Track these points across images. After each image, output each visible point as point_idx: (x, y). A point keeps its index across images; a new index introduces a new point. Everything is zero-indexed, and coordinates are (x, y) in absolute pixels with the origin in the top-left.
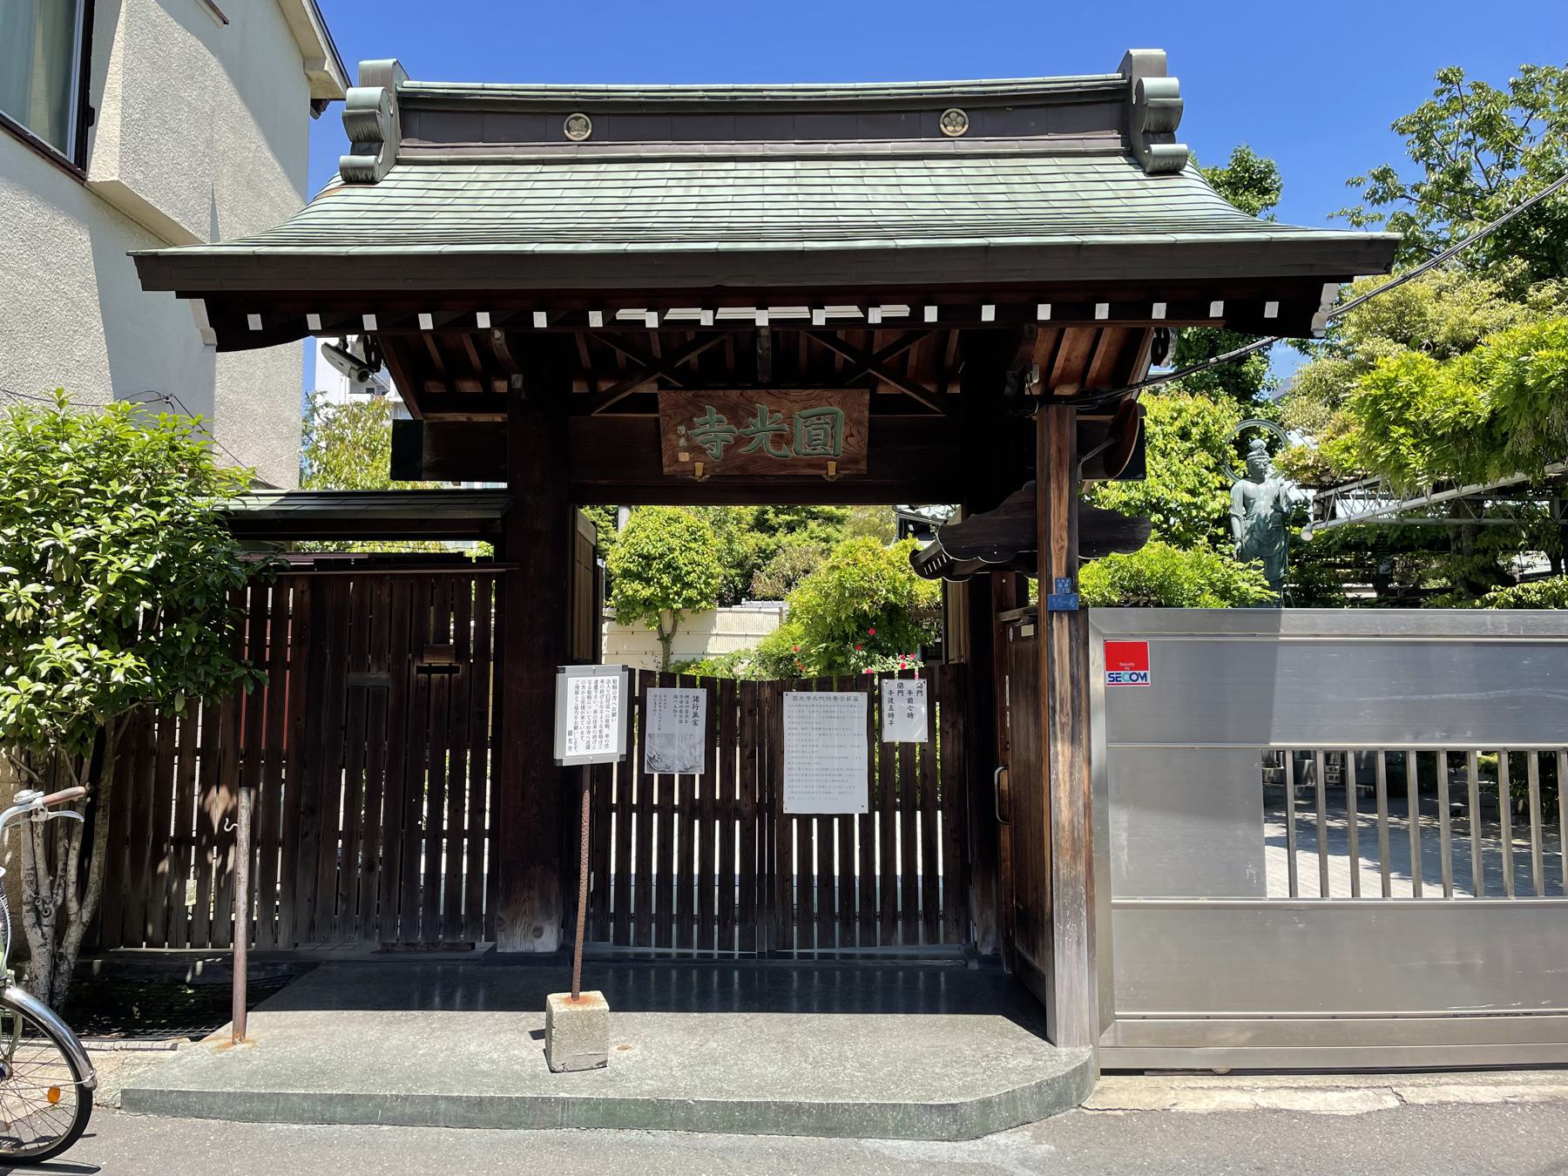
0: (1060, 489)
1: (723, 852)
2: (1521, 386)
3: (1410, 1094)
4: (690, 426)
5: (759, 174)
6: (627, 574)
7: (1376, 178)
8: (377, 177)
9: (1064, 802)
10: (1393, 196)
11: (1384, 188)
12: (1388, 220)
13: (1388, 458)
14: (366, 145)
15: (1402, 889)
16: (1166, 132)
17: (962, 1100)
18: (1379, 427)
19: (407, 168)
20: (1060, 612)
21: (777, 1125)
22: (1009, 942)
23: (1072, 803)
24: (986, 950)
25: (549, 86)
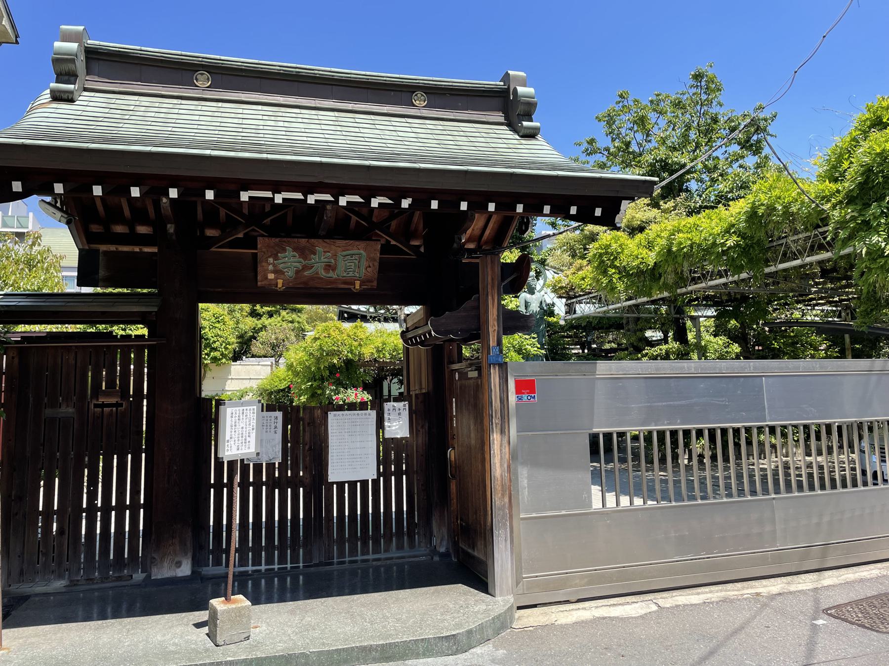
0: (493, 300)
1: (293, 505)
2: (669, 251)
3: (661, 602)
4: (276, 258)
5: (316, 117)
7: (588, 143)
8: (75, 98)
9: (498, 465)
10: (596, 152)
11: (591, 149)
12: (592, 163)
13: (607, 286)
14: (66, 78)
15: (625, 501)
16: (529, 117)
17: (458, 631)
18: (602, 269)
19: (92, 94)
20: (494, 364)
21: (358, 659)
22: (455, 544)
23: (501, 465)
24: (442, 550)
25: (184, 53)
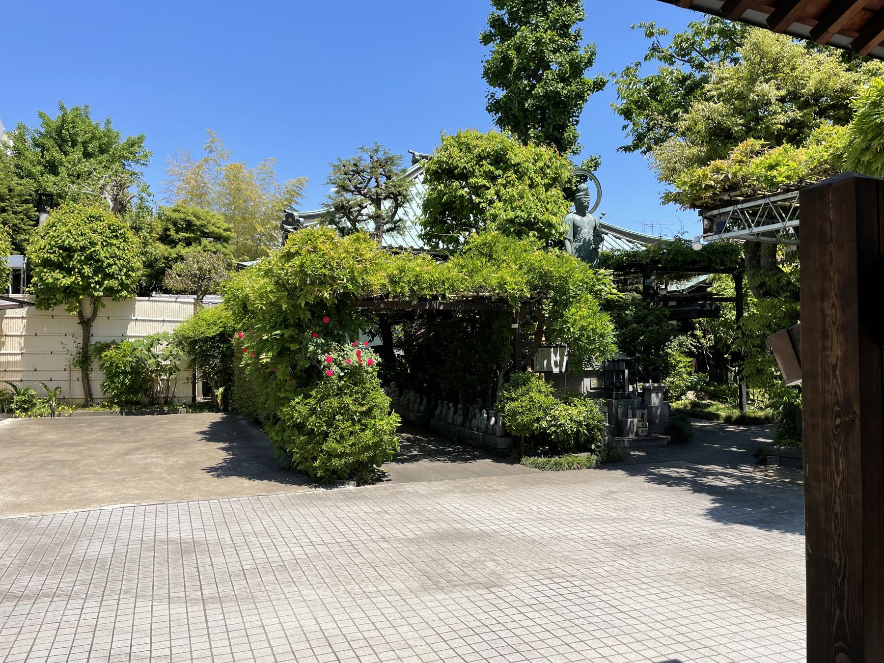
6: (47, 263)
